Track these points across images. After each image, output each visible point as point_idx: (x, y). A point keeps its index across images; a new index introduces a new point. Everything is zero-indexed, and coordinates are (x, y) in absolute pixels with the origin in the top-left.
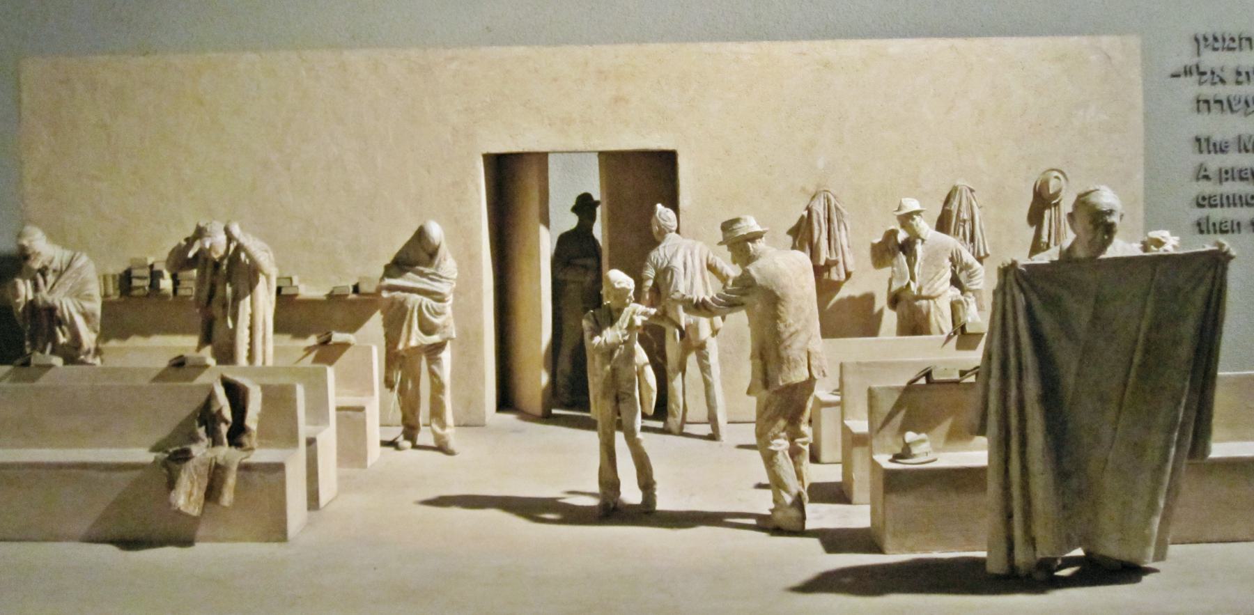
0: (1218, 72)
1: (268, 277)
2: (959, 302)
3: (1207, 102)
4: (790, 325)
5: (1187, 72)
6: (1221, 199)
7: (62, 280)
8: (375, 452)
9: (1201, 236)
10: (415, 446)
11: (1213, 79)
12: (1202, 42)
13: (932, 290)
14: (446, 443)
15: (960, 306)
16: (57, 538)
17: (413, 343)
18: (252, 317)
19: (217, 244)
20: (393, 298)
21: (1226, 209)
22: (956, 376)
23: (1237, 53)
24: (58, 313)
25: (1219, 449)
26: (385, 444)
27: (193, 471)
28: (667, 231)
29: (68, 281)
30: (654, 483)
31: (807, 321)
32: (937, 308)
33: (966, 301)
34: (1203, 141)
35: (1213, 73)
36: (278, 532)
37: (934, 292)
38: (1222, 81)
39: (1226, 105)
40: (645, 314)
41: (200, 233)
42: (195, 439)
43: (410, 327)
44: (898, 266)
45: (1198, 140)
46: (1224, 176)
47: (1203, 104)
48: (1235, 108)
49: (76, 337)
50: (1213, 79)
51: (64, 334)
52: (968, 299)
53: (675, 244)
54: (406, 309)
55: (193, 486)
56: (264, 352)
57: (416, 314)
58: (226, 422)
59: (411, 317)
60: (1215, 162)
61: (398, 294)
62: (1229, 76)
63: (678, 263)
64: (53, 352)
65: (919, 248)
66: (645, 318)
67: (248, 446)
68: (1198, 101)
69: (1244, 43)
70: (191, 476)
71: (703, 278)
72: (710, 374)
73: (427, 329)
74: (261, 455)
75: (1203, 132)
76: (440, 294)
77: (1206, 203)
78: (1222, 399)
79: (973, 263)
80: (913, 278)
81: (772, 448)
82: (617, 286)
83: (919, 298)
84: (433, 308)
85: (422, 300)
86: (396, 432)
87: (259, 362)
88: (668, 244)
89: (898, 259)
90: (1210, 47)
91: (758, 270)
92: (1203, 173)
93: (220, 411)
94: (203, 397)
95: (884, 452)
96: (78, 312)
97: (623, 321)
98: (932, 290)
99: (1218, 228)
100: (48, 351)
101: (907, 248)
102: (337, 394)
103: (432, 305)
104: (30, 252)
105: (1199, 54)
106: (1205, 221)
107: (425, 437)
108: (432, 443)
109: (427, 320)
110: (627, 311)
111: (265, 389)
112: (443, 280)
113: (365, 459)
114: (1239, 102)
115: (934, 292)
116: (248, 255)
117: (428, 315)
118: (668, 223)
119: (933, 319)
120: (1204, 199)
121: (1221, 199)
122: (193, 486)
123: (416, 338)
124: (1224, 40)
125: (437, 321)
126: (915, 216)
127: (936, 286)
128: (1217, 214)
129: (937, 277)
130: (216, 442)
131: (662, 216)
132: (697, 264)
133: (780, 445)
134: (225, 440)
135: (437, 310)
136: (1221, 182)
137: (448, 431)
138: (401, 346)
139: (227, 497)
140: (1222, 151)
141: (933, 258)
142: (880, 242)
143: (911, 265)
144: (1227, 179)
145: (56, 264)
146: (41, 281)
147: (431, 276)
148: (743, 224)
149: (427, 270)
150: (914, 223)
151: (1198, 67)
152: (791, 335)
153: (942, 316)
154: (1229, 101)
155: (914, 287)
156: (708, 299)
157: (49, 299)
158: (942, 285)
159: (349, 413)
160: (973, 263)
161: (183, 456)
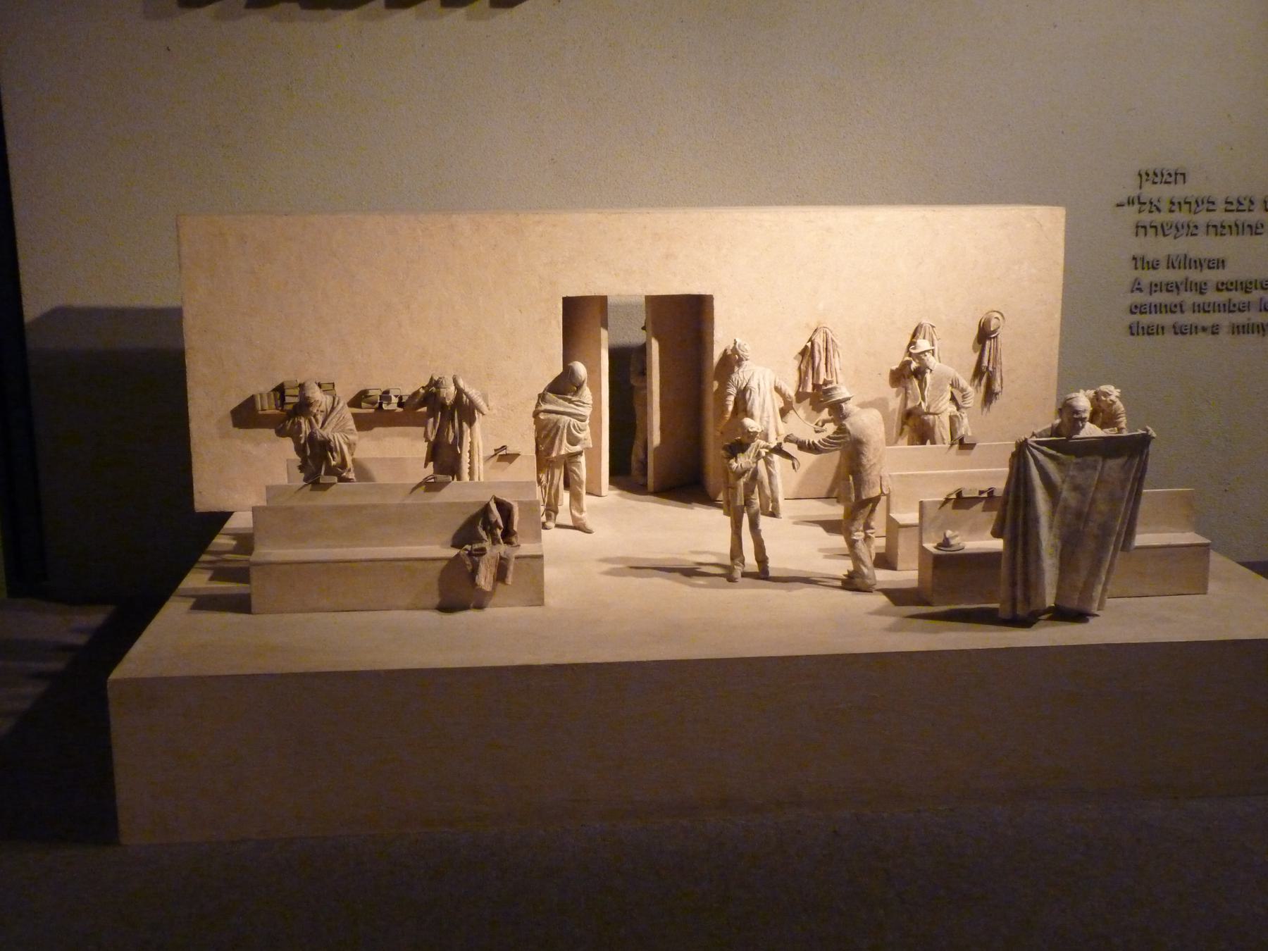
0: (1155, 202)
2: (956, 416)
3: (1144, 227)
4: (870, 460)
5: (1130, 202)
6: (1150, 307)
9: (1132, 337)
11: (1151, 208)
12: (1144, 177)
13: (937, 408)
15: (956, 420)
17: (563, 452)
20: (549, 419)
22: (976, 495)
23: (1172, 185)
25: (1142, 539)
27: (487, 562)
28: (744, 359)
29: (333, 419)
30: (767, 558)
31: (880, 456)
32: (941, 421)
33: (961, 416)
34: (1138, 259)
35: (1151, 203)
37: (938, 410)
38: (1159, 210)
39: (1160, 230)
43: (561, 441)
44: (912, 389)
45: (1134, 258)
46: (1154, 288)
47: (1140, 228)
48: (1167, 232)
49: (343, 459)
50: (1151, 208)
51: (333, 458)
52: (963, 415)
53: (750, 370)
54: (558, 428)
55: (487, 573)
59: (562, 433)
60: (1148, 276)
61: (554, 416)
62: (1165, 206)
63: (753, 384)
65: (928, 376)
67: (516, 544)
68: (1137, 227)
69: (1180, 178)
70: (486, 566)
71: (772, 396)
72: (773, 468)
74: (526, 548)
75: (1138, 251)
76: (581, 415)
77: (1138, 311)
79: (967, 387)
80: (923, 399)
81: (855, 538)
83: (929, 413)
84: (578, 427)
85: (570, 420)
87: (476, 479)
88: (746, 369)
89: (912, 384)
91: (851, 424)
92: (1136, 286)
93: (496, 521)
95: (930, 542)
96: (345, 443)
97: (751, 452)
98: (937, 408)
101: (920, 373)
103: (577, 425)
105: (1141, 187)
106: (1136, 325)
107: (564, 516)
108: (571, 524)
109: (573, 434)
110: (753, 445)
111: (520, 503)
112: (585, 405)
114: (1171, 227)
115: (938, 410)
116: (467, 396)
117: (572, 428)
118: (745, 354)
119: (937, 430)
120: (1136, 307)
121: (1150, 307)
122: (487, 573)
124: (1162, 175)
125: (581, 436)
126: (926, 354)
127: (940, 405)
128: (1146, 319)
129: (941, 398)
130: (495, 541)
131: (741, 348)
132: (767, 387)
133: (859, 536)
134: (501, 541)
135: (581, 428)
136: (1151, 294)
137: (584, 515)
138: (554, 455)
140: (1154, 268)
141: (938, 384)
142: (897, 369)
143: (922, 390)
144: (1155, 291)
146: (313, 420)
147: (576, 403)
148: (839, 391)
149: (574, 399)
150: (925, 358)
151: (1139, 198)
152: (871, 466)
153: (944, 428)
155: (924, 406)
156: (816, 442)
157: (324, 433)
158: (944, 404)
160: (967, 387)
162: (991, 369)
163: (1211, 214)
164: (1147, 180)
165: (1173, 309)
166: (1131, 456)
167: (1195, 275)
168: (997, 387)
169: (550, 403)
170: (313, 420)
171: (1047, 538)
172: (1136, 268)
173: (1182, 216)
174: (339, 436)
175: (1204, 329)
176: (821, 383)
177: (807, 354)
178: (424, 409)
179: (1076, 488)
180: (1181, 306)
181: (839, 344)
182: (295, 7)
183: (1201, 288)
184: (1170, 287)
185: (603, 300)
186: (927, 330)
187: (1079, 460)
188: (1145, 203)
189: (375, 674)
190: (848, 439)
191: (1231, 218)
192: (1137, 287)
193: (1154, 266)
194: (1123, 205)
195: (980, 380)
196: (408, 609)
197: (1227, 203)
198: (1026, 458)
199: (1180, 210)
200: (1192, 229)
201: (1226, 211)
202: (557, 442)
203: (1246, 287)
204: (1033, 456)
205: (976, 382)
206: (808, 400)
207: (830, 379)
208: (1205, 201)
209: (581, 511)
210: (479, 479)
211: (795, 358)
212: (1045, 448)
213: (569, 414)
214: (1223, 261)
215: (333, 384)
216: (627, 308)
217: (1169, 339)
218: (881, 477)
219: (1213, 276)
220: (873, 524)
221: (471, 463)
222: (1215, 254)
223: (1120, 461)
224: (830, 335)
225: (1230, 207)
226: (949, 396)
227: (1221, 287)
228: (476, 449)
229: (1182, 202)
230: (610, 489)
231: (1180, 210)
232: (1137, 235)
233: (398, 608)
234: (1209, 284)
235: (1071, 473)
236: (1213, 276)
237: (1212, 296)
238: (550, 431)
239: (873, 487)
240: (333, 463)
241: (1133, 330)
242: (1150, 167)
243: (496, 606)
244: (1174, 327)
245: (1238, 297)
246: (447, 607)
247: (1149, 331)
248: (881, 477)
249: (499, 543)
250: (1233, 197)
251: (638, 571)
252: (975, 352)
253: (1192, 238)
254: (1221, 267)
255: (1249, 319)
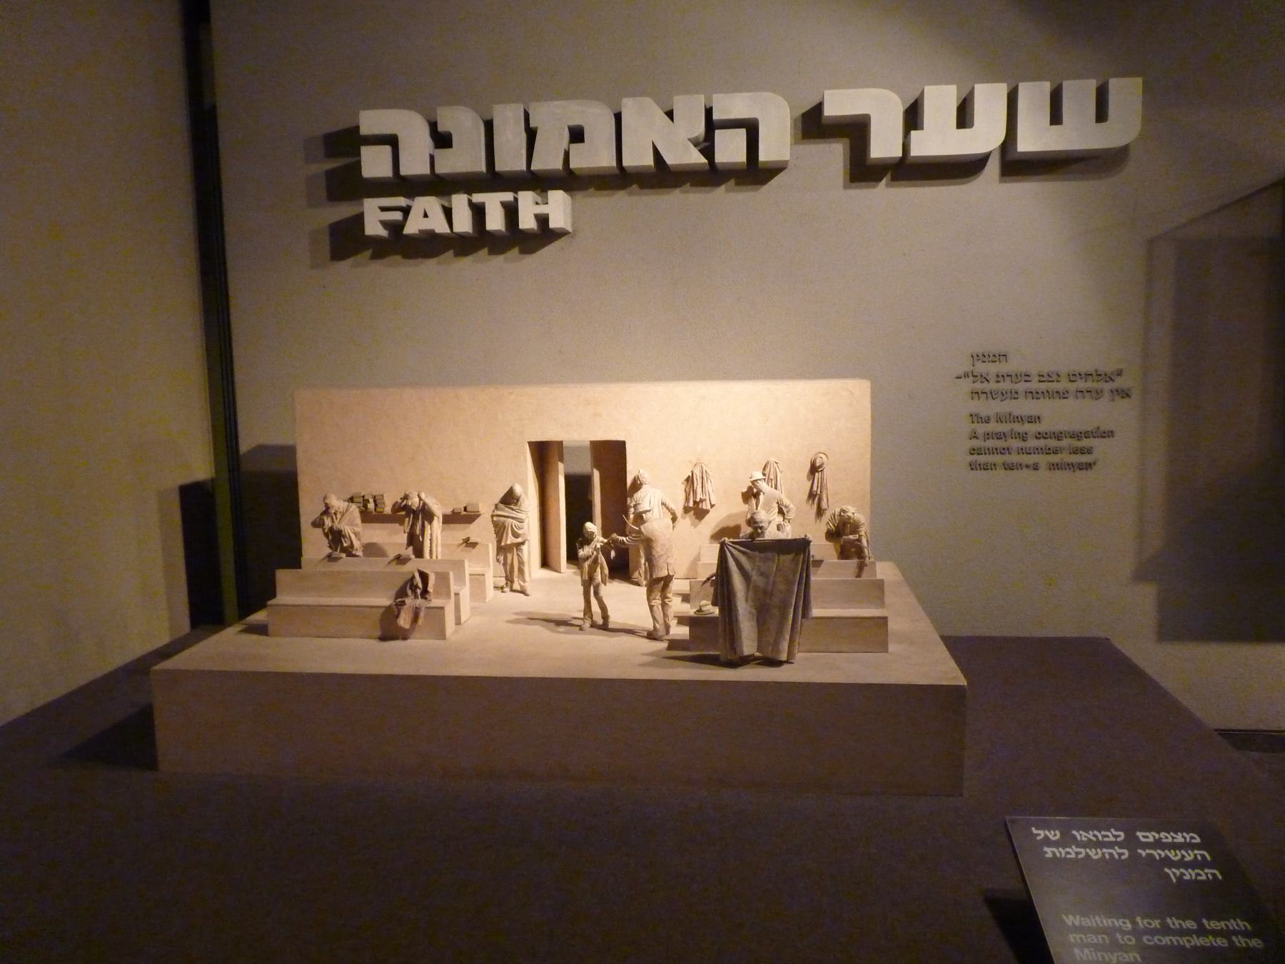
0: (984, 375)
1: (438, 518)
7: (344, 517)
8: (491, 593)
10: (512, 590)
12: (975, 357)
14: (525, 590)
16: (349, 637)
17: (509, 542)
18: (431, 535)
19: (414, 502)
20: (499, 521)
21: (987, 455)
24: (343, 533)
25: (816, 612)
26: (496, 588)
29: (347, 518)
35: (982, 376)
36: (441, 635)
39: (992, 395)
40: (602, 542)
41: (406, 497)
42: (406, 595)
43: (507, 534)
45: (972, 415)
47: (975, 394)
48: (994, 397)
49: (352, 546)
51: (345, 542)
54: (505, 526)
56: (437, 551)
57: (510, 528)
58: (420, 589)
60: (981, 429)
62: (992, 378)
64: (341, 551)
65: (761, 497)
66: (602, 544)
73: (516, 535)
75: (974, 411)
78: (813, 594)
81: (652, 604)
82: (589, 530)
86: (502, 582)
87: (434, 557)
90: (981, 361)
93: (417, 584)
94: (410, 577)
96: (352, 533)
97: (593, 545)
99: (982, 467)
100: (338, 550)
101: (756, 496)
102: (469, 566)
104: (330, 506)
107: (516, 586)
108: (519, 588)
111: (437, 574)
113: (485, 598)
117: (516, 529)
123: (510, 540)
125: (520, 532)
128: (982, 459)
130: (416, 597)
134: (419, 597)
136: (985, 440)
137: (526, 584)
138: (503, 544)
139: (420, 621)
143: (757, 506)
145: (341, 510)
146: (334, 517)
148: (641, 506)
149: (515, 508)
151: (972, 373)
154: (991, 393)
159: (478, 577)
161: (403, 603)
162: (819, 492)
163: (1028, 384)
164: (978, 360)
165: (1002, 451)
166: (797, 554)
167: (1018, 428)
168: (824, 505)
169: (501, 510)
170: (334, 517)
171: (743, 607)
172: (973, 422)
173: (1006, 385)
174: (349, 529)
175: (1027, 466)
176: (698, 500)
177: (690, 480)
178: (404, 513)
179: (762, 574)
180: (1008, 449)
181: (710, 473)
182: (398, 258)
183: (1024, 437)
184: (1000, 436)
185: (560, 443)
186: (772, 465)
187: (762, 555)
188: (976, 376)
189: (244, 675)
190: (642, 538)
191: (1043, 386)
192: (974, 436)
193: (987, 421)
194: (960, 378)
195: (814, 500)
196: (361, 638)
197: (1040, 376)
198: (725, 551)
199: (1004, 381)
200: (1035, 395)
201: (1040, 381)
202: (504, 536)
203: (1058, 436)
204: (730, 552)
205: (811, 501)
206: (692, 512)
207: (704, 498)
208: (1023, 375)
209: (524, 581)
210: (437, 558)
211: (682, 483)
212: (738, 547)
213: (513, 518)
214: (1039, 418)
215: (383, 496)
216: (577, 449)
217: (1001, 472)
218: (668, 564)
219: (1032, 428)
220: (669, 595)
221: (431, 547)
222: (1035, 413)
223: (790, 557)
224: (705, 468)
225: (1042, 379)
226: (777, 510)
227: (1039, 436)
228: (434, 538)
229: (1005, 376)
230: (568, 568)
231: (1004, 381)
232: (972, 399)
233: (355, 637)
234: (1029, 434)
235: (757, 564)
236: (1032, 428)
237: (1032, 443)
238: (500, 529)
239: (661, 570)
240: (345, 545)
241: (973, 466)
242: (980, 351)
243: (415, 638)
244: (1004, 465)
245: (1052, 443)
246: (383, 638)
247: (985, 467)
248: (668, 564)
249: (418, 598)
250: (1045, 371)
251: (533, 621)
252: (809, 480)
253: (1013, 401)
254: (1038, 423)
255: (1062, 460)
